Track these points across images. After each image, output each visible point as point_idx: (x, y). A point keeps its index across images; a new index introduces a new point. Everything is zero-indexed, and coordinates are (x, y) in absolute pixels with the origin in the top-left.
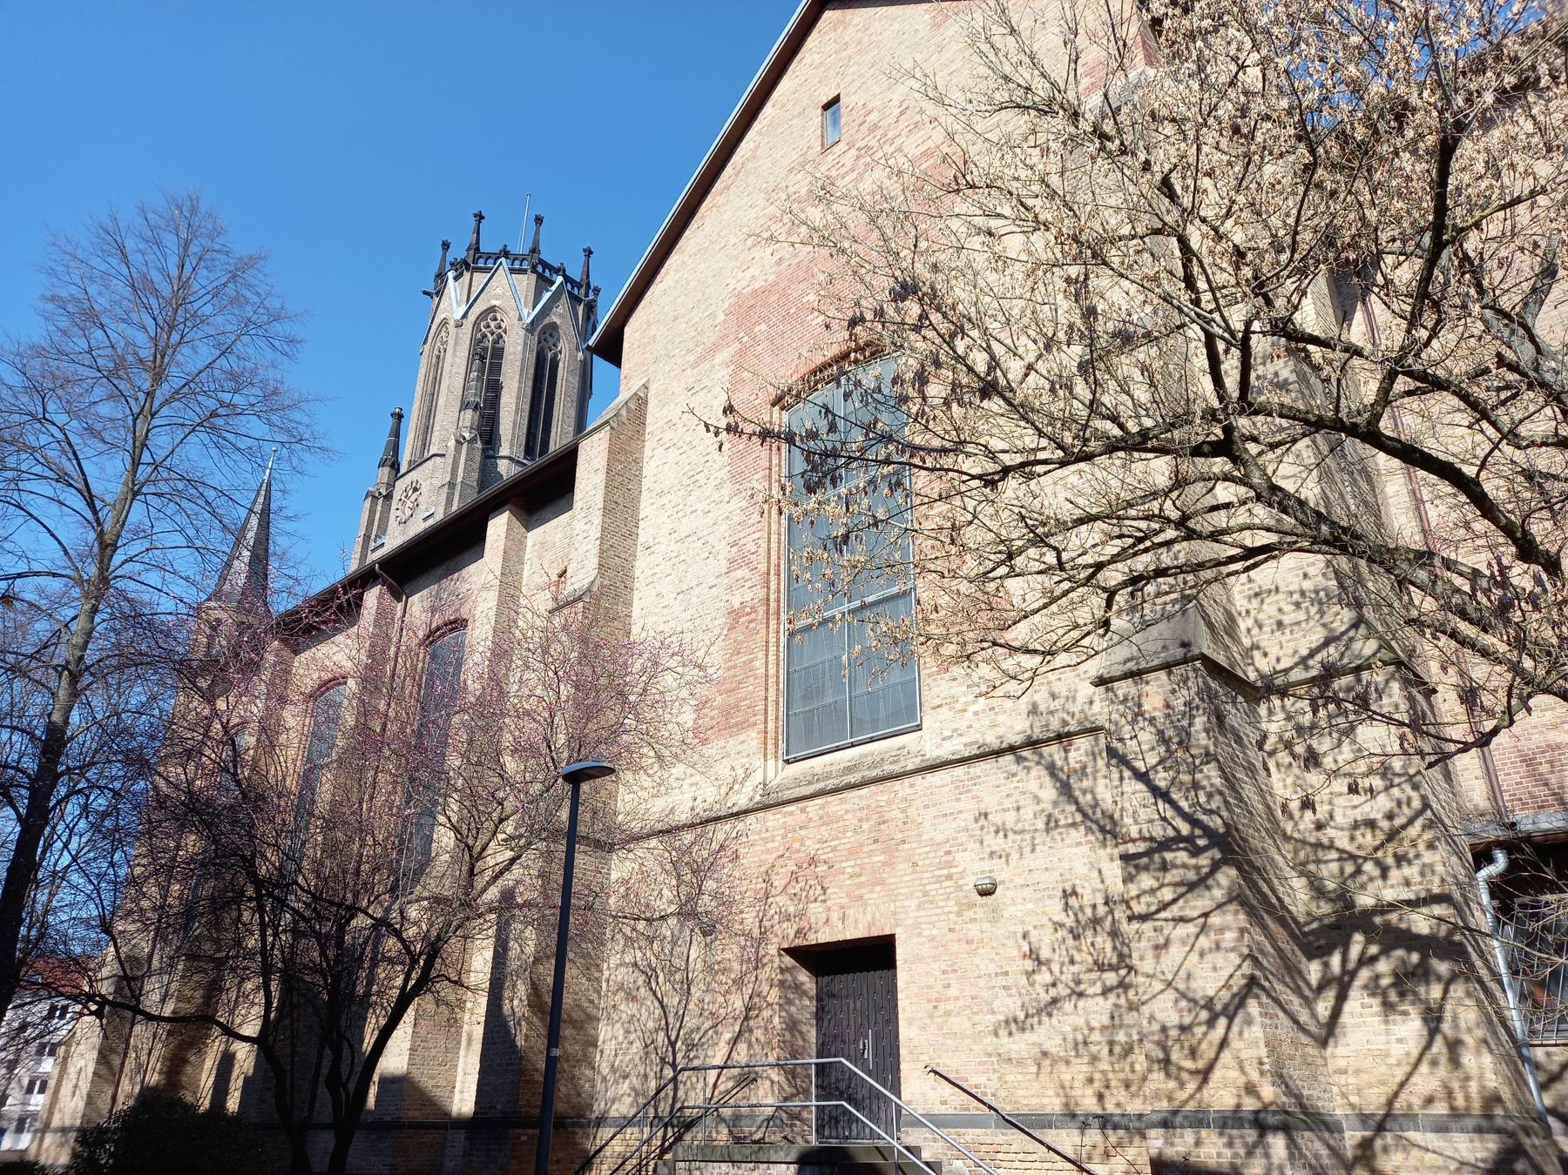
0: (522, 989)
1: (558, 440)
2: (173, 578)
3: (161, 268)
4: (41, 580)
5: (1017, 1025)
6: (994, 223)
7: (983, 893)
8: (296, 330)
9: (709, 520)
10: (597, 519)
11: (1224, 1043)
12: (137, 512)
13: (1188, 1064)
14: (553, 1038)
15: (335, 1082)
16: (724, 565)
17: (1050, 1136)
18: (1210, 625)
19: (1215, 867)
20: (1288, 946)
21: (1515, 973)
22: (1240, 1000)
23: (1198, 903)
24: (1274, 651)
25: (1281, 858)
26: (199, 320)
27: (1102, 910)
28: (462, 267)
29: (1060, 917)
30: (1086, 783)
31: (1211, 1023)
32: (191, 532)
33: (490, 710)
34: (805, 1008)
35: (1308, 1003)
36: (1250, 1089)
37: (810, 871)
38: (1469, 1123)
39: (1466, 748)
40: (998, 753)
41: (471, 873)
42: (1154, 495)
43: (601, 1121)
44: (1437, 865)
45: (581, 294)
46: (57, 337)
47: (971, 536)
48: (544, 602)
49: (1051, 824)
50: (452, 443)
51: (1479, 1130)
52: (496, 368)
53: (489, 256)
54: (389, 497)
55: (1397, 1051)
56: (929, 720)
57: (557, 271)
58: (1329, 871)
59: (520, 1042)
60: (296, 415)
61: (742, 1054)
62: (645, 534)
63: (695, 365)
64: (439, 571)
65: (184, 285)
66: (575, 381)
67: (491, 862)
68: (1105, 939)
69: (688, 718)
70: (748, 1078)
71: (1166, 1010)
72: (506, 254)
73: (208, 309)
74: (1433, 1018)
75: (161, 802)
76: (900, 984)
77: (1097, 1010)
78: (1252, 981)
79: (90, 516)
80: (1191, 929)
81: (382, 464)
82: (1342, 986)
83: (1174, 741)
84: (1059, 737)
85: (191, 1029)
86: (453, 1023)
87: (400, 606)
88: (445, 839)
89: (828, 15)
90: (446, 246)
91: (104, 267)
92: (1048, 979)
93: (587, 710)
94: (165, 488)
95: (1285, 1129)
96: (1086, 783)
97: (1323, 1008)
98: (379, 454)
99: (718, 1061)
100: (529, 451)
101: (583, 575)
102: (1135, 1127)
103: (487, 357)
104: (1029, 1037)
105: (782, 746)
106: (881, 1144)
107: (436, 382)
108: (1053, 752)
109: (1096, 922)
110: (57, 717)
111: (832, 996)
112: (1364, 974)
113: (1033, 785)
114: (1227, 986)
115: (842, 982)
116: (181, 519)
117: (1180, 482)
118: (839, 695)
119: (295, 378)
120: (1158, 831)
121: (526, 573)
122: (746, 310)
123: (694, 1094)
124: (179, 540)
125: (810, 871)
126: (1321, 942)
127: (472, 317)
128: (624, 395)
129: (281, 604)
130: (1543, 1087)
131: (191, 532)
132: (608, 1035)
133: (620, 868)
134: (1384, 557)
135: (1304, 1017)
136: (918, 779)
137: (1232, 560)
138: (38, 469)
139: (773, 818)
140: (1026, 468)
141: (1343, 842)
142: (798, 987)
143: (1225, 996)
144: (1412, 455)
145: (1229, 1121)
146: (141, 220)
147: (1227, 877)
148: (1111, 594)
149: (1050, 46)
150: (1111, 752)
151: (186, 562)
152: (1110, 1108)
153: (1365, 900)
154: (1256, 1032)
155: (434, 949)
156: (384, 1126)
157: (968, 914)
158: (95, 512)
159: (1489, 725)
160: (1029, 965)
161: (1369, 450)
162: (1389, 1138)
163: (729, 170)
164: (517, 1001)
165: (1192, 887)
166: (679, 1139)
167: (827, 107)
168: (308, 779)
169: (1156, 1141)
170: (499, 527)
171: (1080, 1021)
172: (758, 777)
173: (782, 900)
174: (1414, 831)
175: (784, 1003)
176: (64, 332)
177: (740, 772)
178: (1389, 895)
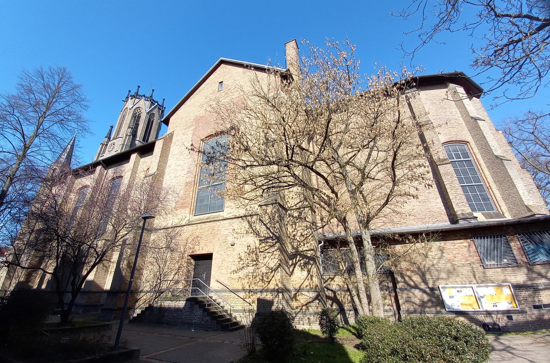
0: (126, 262)
1: (151, 139)
2: (44, 158)
3: (53, 83)
4: (6, 154)
5: (235, 272)
6: (251, 117)
7: (232, 245)
8: (88, 104)
9: (184, 162)
10: (158, 158)
11: (273, 276)
12: (37, 140)
13: (267, 280)
14: (132, 273)
15: (73, 283)
16: (186, 172)
17: (239, 294)
18: (281, 197)
19: (276, 243)
20: (286, 258)
21: (322, 263)
22: (277, 268)
23: (272, 249)
24: (291, 203)
25: (288, 241)
26: (61, 97)
27: (254, 250)
28: (133, 97)
29: (246, 251)
30: (255, 225)
31: (272, 272)
32: (51, 147)
33: (126, 198)
34: (192, 268)
35: (289, 269)
36: (277, 285)
37: (197, 239)
38: (313, 290)
39: (320, 228)
40: (239, 218)
41: (116, 236)
42: (274, 173)
43: (141, 292)
44: (313, 244)
45: (161, 108)
46: (20, 94)
47: (239, 177)
48: (142, 175)
49: (247, 232)
50: (125, 135)
51: (314, 291)
52: (138, 120)
53: (140, 96)
54: (107, 145)
55: (302, 277)
56: (226, 210)
57: (156, 102)
58: (295, 244)
59: (123, 274)
60: (85, 124)
61: (176, 277)
62: (169, 163)
63: (185, 129)
64: (117, 164)
65: (59, 88)
66: (157, 126)
67: (121, 234)
68: (254, 255)
69: (174, 205)
70: (177, 282)
71: (264, 270)
72: (144, 96)
73: (65, 95)
74: (309, 271)
75: (33, 213)
76: (213, 263)
77: (251, 269)
78: (280, 265)
79: (23, 140)
80: (270, 254)
81: (106, 137)
82: (295, 265)
83: (272, 219)
84: (251, 215)
85: (34, 268)
86: (107, 271)
87: (106, 171)
88: (110, 227)
89: (222, 65)
90: (130, 91)
91: (37, 80)
92: (242, 263)
93: (149, 201)
94: (45, 136)
95: (282, 292)
96: (255, 225)
97: (291, 269)
98: (106, 135)
99: (170, 279)
100: (144, 140)
101: (153, 170)
102: (255, 292)
103: (136, 118)
104: (237, 274)
105: (194, 212)
106: (204, 296)
107: (123, 121)
108: (249, 218)
109: (253, 252)
110: (5, 189)
111: (198, 265)
112: (299, 263)
113: (244, 225)
114: (275, 265)
115: (200, 262)
116: (49, 144)
117: (279, 171)
118: (207, 203)
119: (86, 115)
120: (267, 235)
121: (139, 168)
122: (198, 120)
123: (164, 286)
124: (48, 149)
125: (197, 239)
126: (292, 258)
127: (134, 108)
128: (168, 133)
129: (74, 167)
130: (324, 283)
131: (51, 147)
132: (145, 272)
133: (153, 237)
134: (311, 189)
135: (288, 271)
136: (222, 221)
137: (286, 186)
138: (9, 126)
139: (190, 227)
140: (251, 166)
141: (298, 239)
142: (191, 263)
143: (275, 267)
144: (318, 173)
145: (273, 291)
146: (49, 70)
147: (278, 245)
148: (264, 190)
149: (265, 89)
150: (260, 220)
151: (49, 155)
152: (251, 288)
153: (301, 249)
154: (279, 274)
155: (104, 253)
156: (85, 292)
157: (228, 250)
158: (24, 139)
159: (324, 224)
160: (239, 260)
161: (311, 171)
162: (299, 293)
163: (198, 90)
164: (124, 265)
165: (271, 246)
166: (160, 295)
167: (220, 83)
168: (76, 209)
169: (259, 295)
170: (134, 157)
171: (248, 271)
172: (188, 218)
173: (190, 245)
174: (310, 237)
175: (188, 266)
176: (22, 94)
177: (184, 217)
178: (305, 249)
